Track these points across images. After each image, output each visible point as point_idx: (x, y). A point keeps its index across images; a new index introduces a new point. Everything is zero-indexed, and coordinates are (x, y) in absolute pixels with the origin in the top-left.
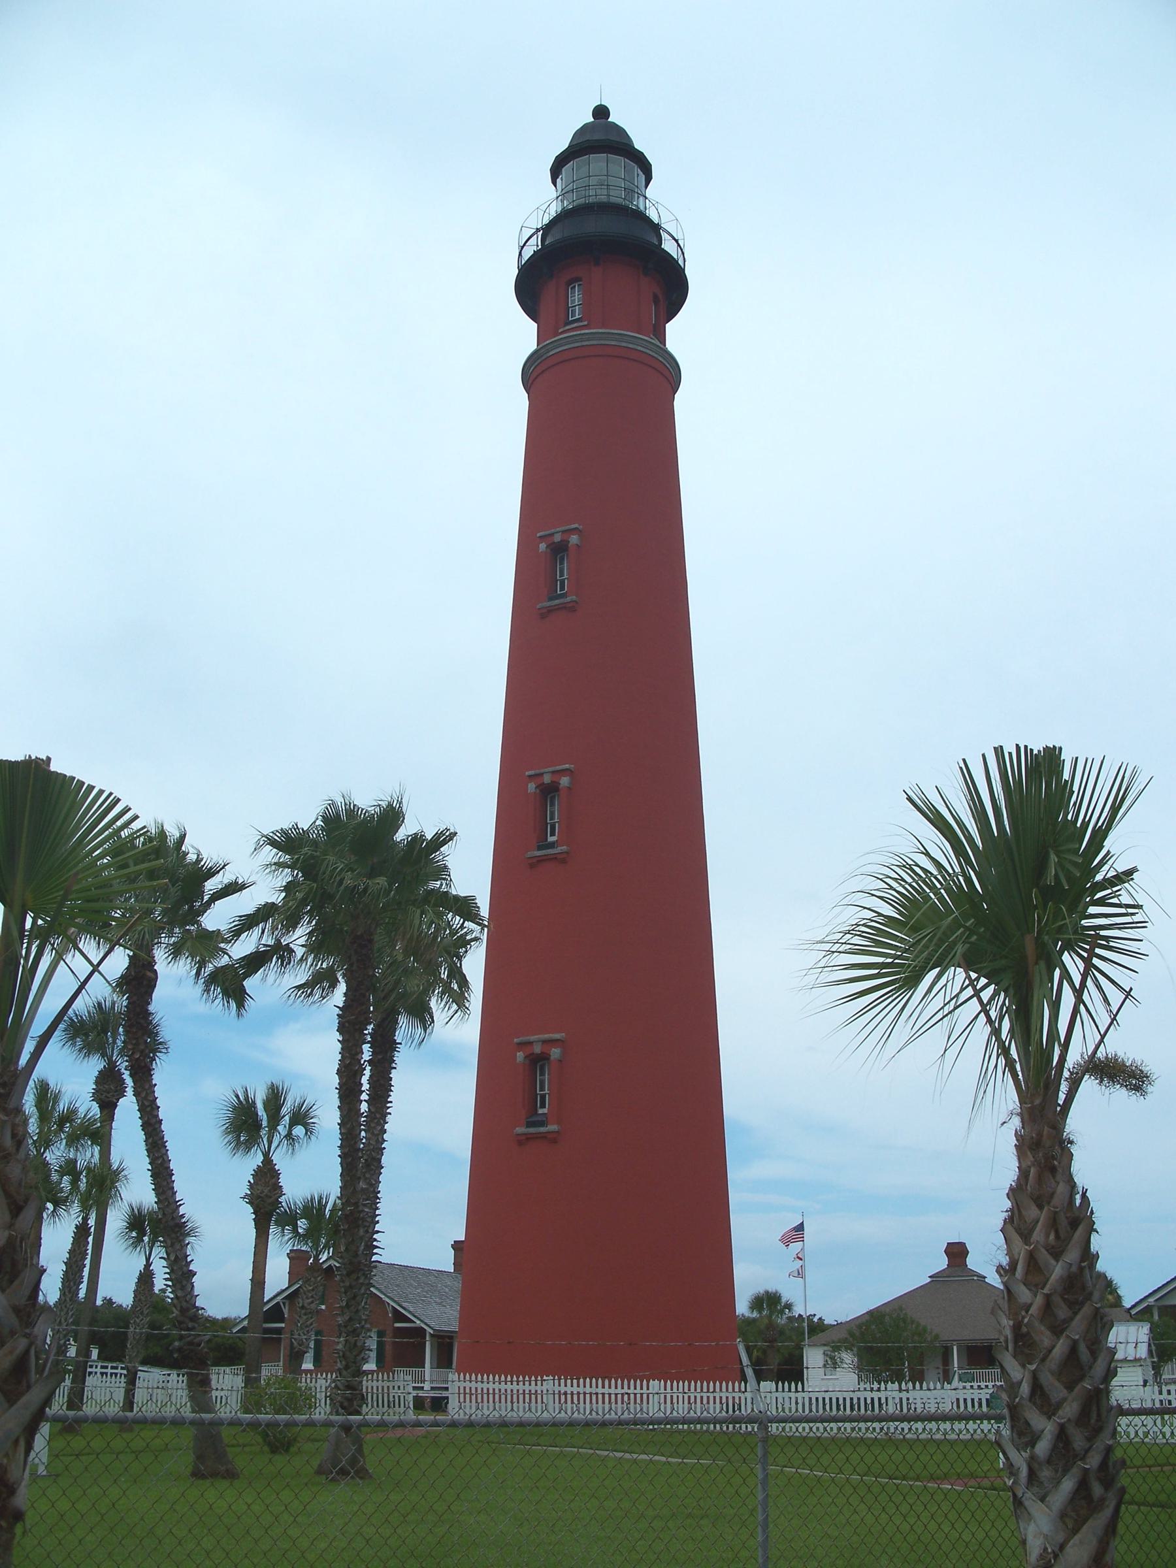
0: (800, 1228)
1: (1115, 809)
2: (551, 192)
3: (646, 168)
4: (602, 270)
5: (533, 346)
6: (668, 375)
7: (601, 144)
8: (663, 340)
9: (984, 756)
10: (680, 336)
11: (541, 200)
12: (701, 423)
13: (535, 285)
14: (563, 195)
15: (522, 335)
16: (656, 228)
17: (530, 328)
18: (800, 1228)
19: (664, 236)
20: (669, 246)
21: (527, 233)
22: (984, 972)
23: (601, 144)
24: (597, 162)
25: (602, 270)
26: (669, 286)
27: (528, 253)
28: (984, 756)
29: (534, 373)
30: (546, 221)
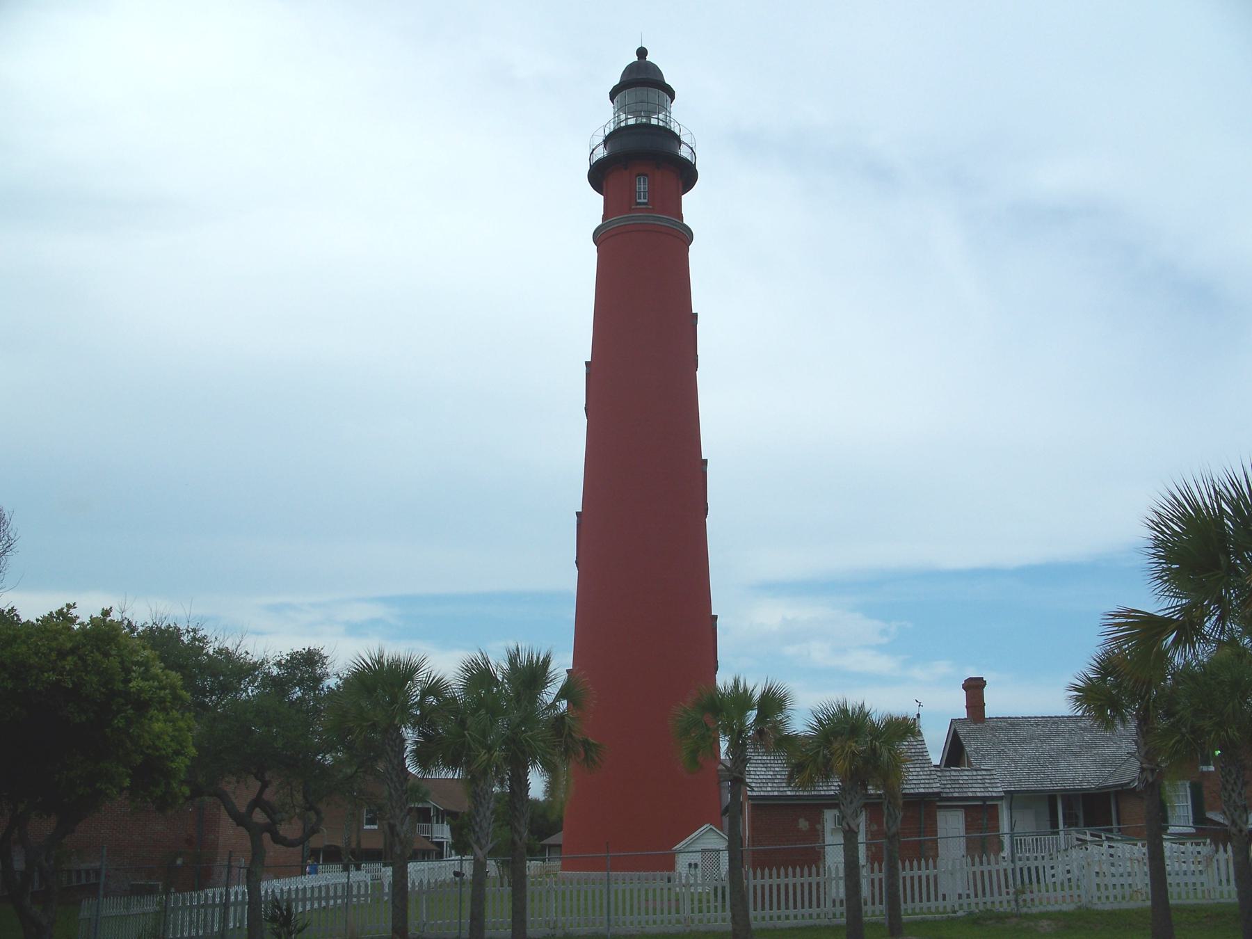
3: (671, 93)
4: (643, 169)
5: (599, 221)
7: (642, 82)
8: (680, 217)
11: (601, 117)
12: (702, 263)
13: (599, 175)
17: (600, 198)
23: (642, 82)
25: (643, 169)
29: (599, 237)
30: (607, 132)
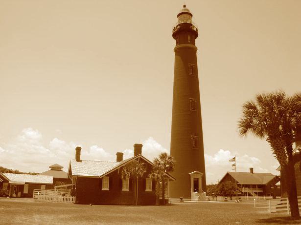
0: (234, 158)
11: (175, 22)
18: (234, 158)
28: (185, 33)
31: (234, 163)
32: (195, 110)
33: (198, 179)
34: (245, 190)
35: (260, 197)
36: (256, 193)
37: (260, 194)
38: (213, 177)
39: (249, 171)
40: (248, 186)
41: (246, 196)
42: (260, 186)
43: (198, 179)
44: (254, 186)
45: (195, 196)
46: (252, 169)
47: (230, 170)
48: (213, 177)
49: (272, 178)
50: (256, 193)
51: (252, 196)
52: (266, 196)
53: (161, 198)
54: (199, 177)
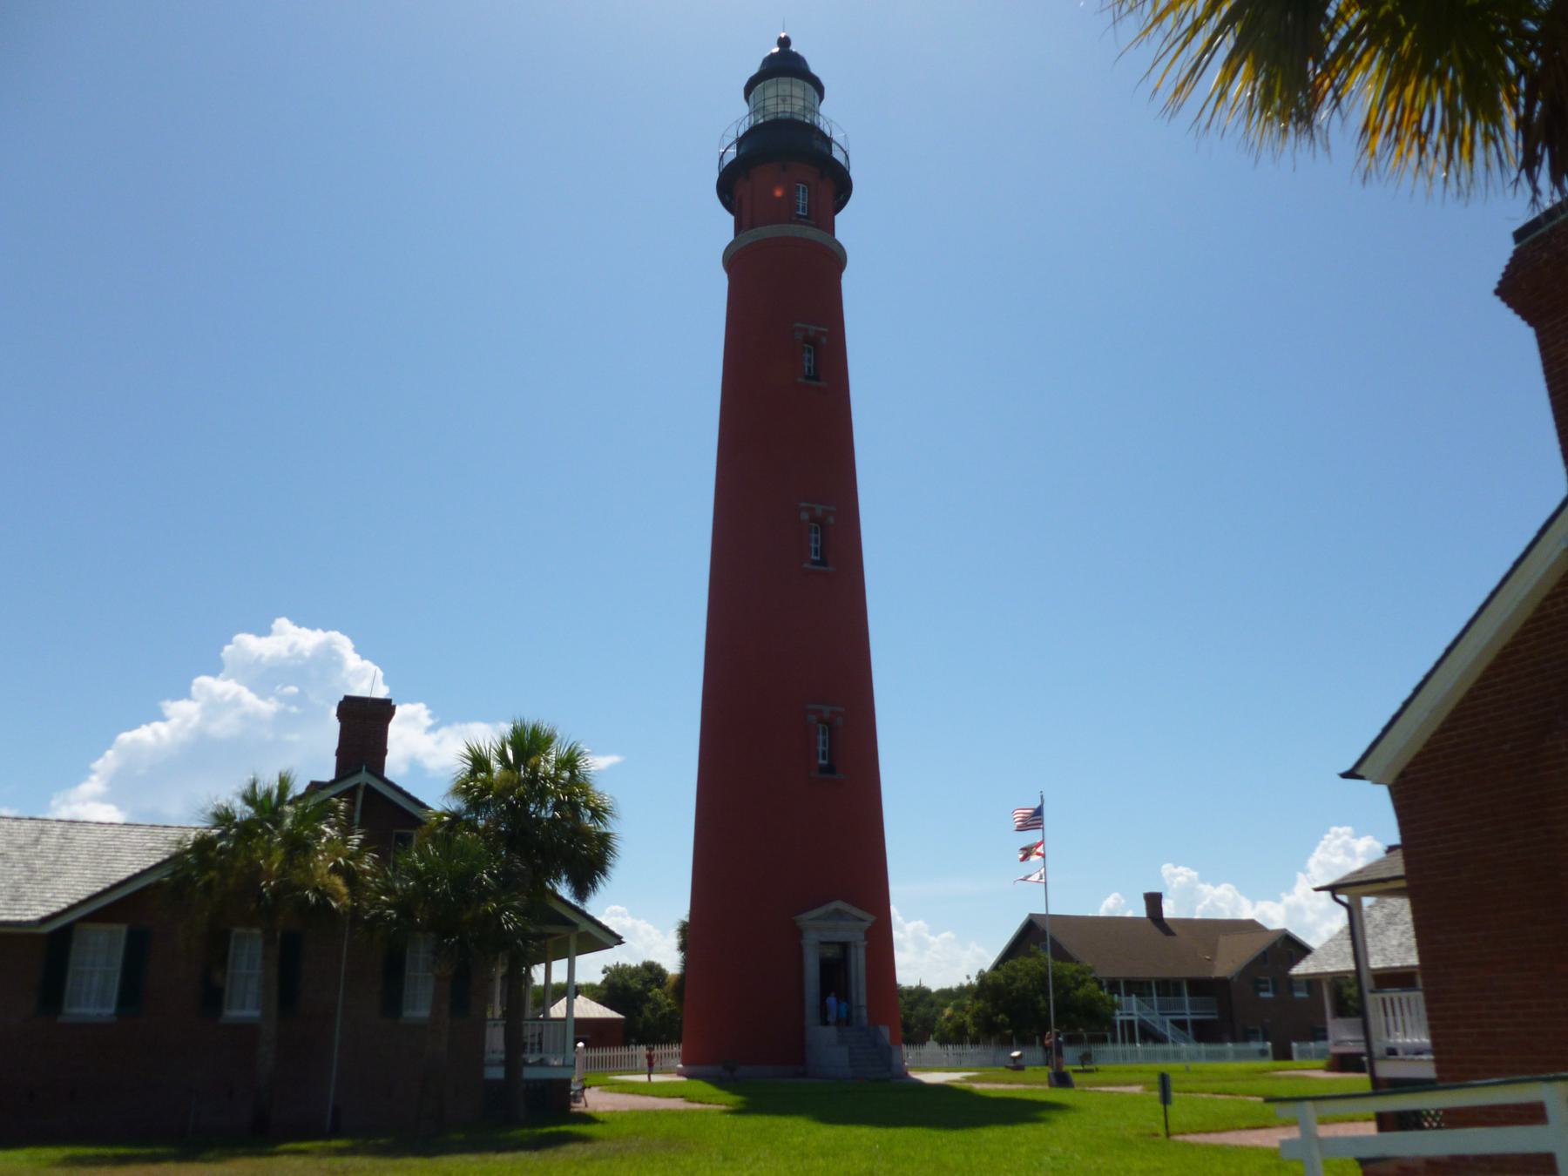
0: (1039, 812)
1: (1183, 85)
2: (744, 109)
3: (819, 88)
6: (836, 260)
7: (785, 65)
9: (784, 176)
10: (848, 226)
11: (732, 117)
14: (753, 112)
15: (721, 227)
16: (828, 141)
17: (728, 220)
18: (1039, 812)
19: (834, 146)
20: (837, 155)
21: (728, 141)
22: (573, 948)
24: (785, 86)
26: (836, 185)
27: (727, 160)
28: (784, 176)
29: (735, 261)
31: (1032, 837)
32: (831, 569)
33: (845, 947)
34: (1131, 1009)
35: (1203, 1047)
36: (1181, 1024)
37: (1205, 1033)
38: (940, 942)
39: (1139, 910)
40: (1137, 987)
41: (1132, 1041)
42: (1202, 987)
43: (845, 947)
44: (1168, 987)
45: (175, 721)
46: (1154, 901)
47: (1040, 910)
48: (940, 942)
49: (1257, 946)
50: (1181, 1024)
51: (1160, 1039)
52: (1234, 1040)
53: (497, 1073)
54: (854, 933)
